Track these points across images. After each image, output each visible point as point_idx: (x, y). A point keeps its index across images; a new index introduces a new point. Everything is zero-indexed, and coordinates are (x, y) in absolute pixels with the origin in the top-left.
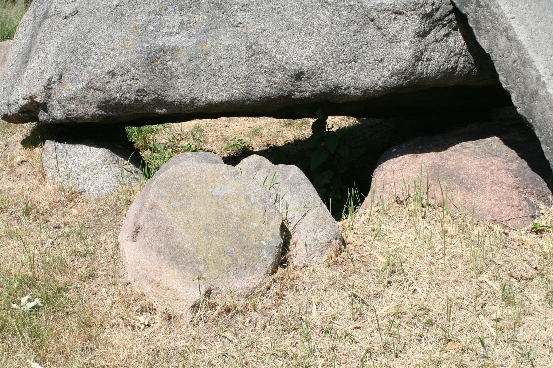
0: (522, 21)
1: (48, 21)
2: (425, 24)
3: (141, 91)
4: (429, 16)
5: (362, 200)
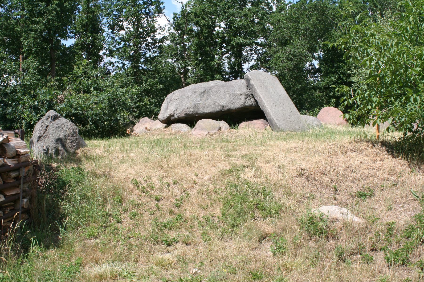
0: (262, 94)
1: (171, 102)
2: (246, 96)
3: (193, 111)
4: (247, 95)
5: (197, 83)
